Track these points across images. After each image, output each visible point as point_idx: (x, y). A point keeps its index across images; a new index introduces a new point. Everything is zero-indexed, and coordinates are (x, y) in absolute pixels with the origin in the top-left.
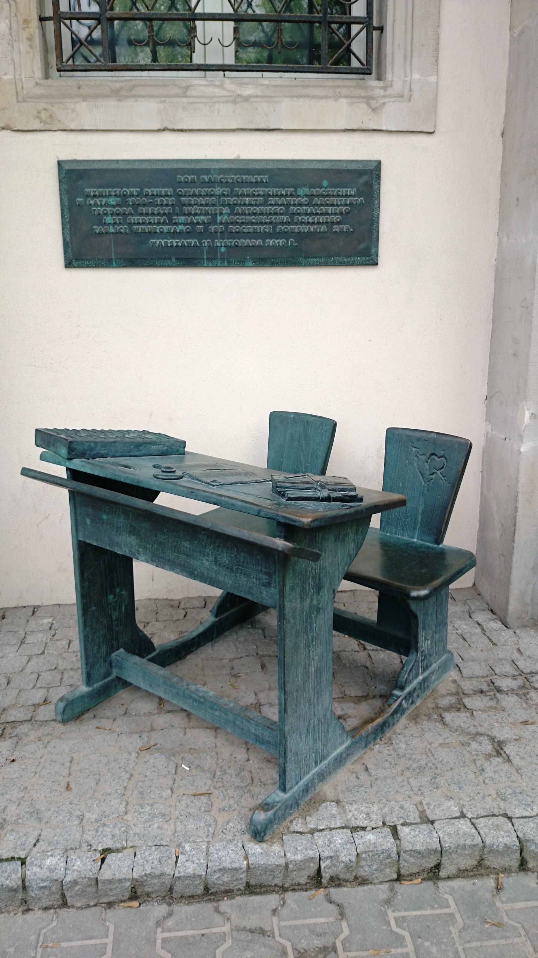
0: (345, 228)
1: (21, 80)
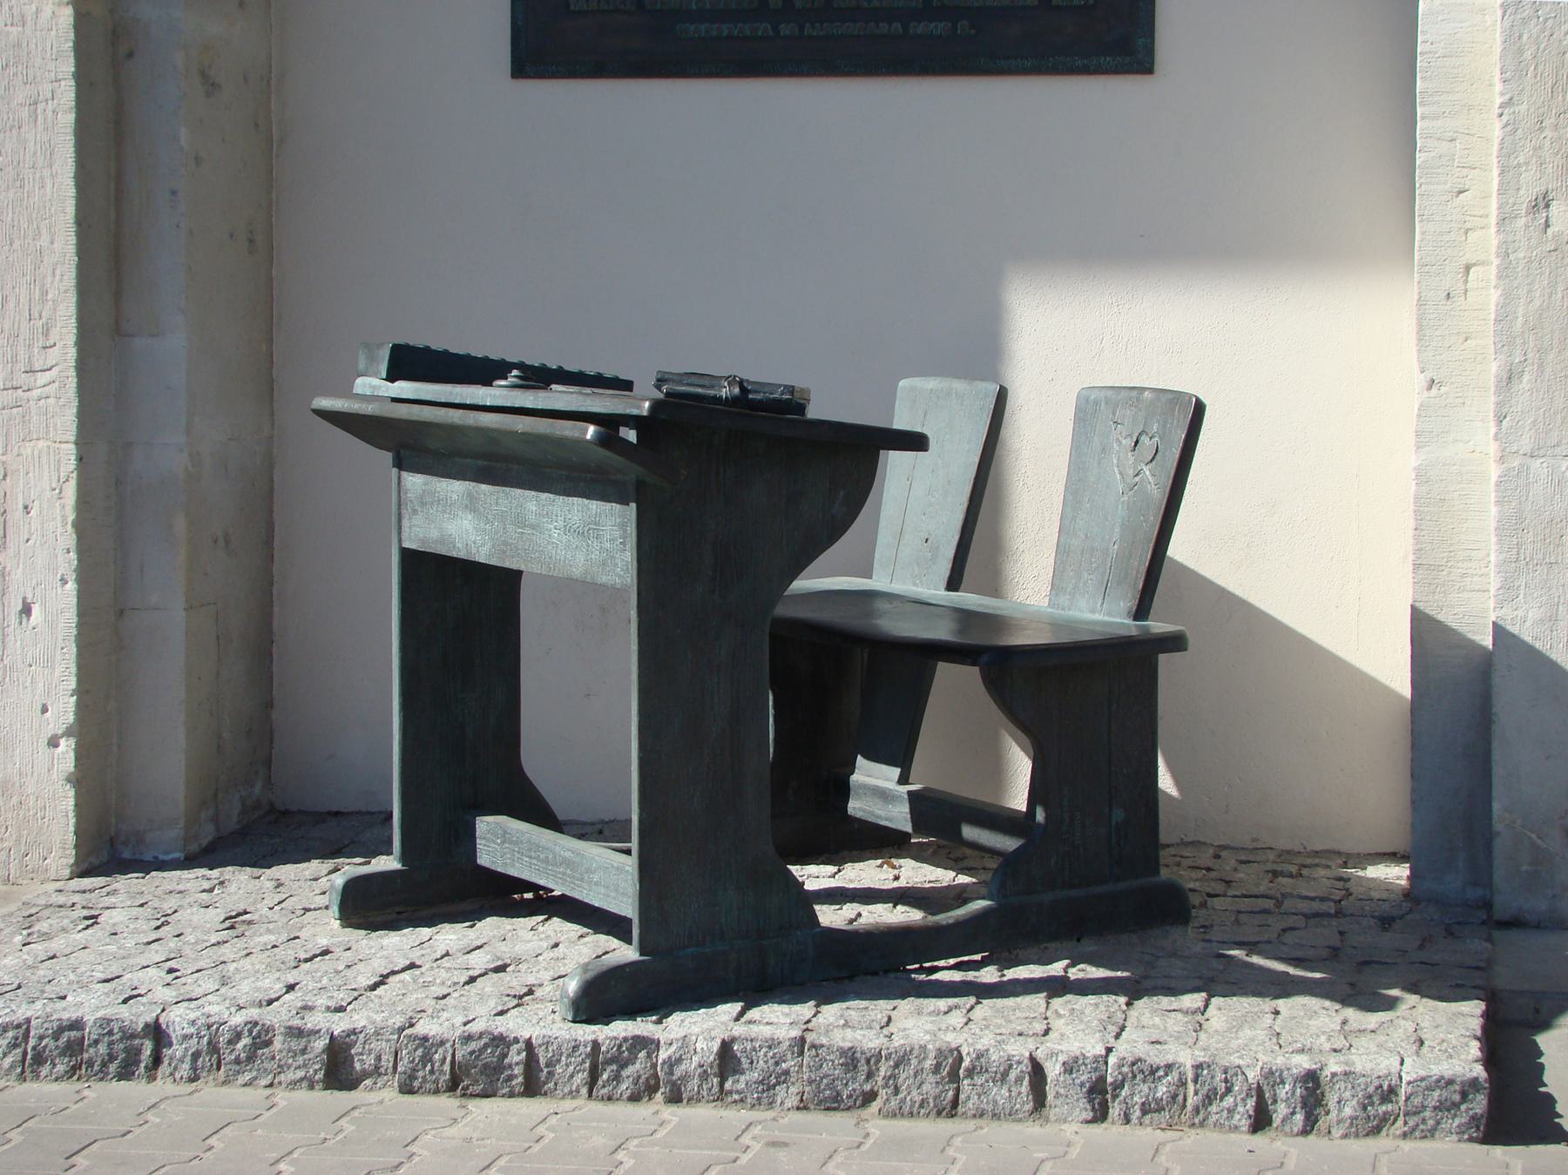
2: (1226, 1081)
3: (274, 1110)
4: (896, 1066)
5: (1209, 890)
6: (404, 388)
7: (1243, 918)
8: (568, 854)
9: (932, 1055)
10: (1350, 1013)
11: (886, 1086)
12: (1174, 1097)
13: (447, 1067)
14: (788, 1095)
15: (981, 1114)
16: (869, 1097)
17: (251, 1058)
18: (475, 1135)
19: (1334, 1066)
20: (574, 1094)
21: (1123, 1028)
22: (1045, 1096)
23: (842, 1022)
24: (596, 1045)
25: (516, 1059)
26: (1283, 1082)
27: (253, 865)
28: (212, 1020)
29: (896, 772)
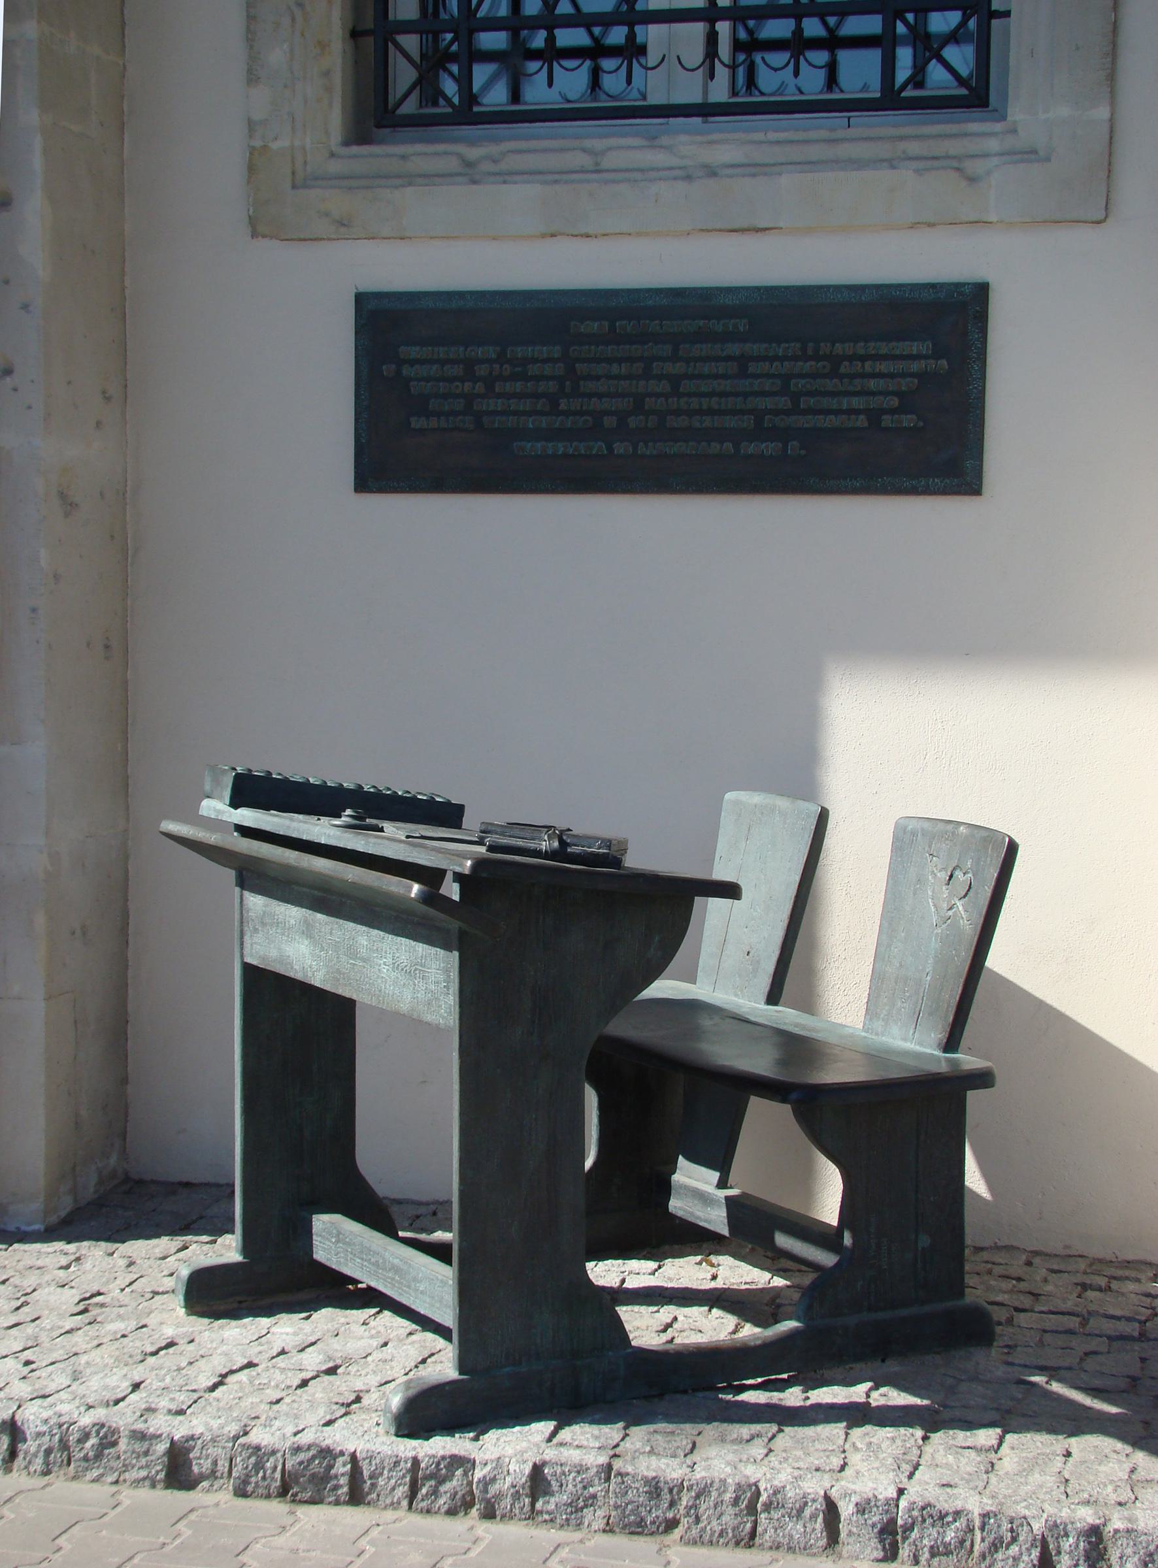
0: (908, 420)
1: (304, 148)
2: (1012, 1530)
3: (119, 1509)
4: (698, 1496)
5: (1017, 1304)
6: (248, 816)
7: (1048, 1338)
8: (396, 1261)
9: (732, 1488)
10: (1140, 1457)
11: (688, 1515)
12: (962, 1542)
13: (278, 1475)
14: (595, 1518)
16: (672, 1524)
17: (99, 1456)
18: (302, 1547)
19: (1117, 1523)
20: (395, 1506)
21: (916, 1467)
22: (838, 1533)
23: (648, 1449)
24: (416, 1462)
25: (342, 1470)
26: (1067, 1535)
27: (108, 1239)
28: (63, 1419)
29: (715, 1176)
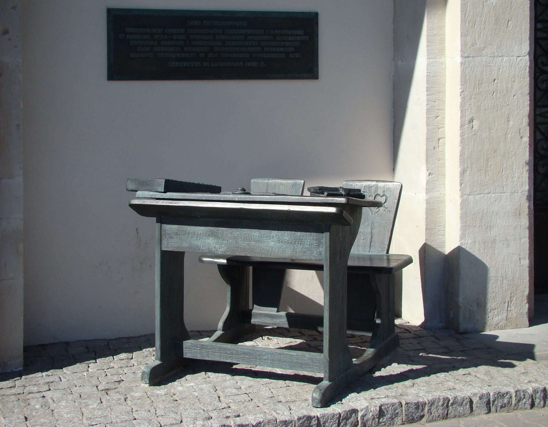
0: (297, 55)
4: (431, 406)
12: (509, 402)
15: (455, 417)
16: (422, 417)
25: (314, 423)
